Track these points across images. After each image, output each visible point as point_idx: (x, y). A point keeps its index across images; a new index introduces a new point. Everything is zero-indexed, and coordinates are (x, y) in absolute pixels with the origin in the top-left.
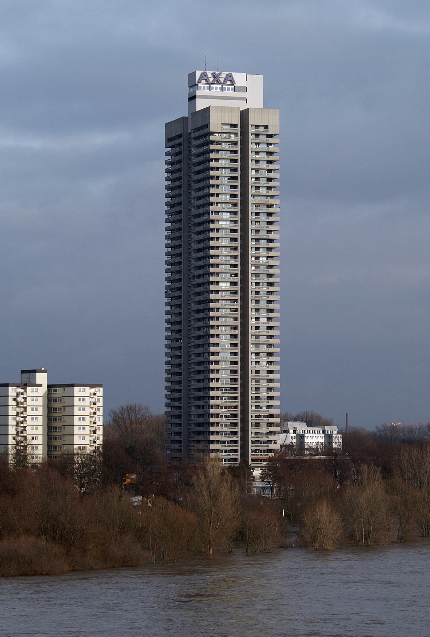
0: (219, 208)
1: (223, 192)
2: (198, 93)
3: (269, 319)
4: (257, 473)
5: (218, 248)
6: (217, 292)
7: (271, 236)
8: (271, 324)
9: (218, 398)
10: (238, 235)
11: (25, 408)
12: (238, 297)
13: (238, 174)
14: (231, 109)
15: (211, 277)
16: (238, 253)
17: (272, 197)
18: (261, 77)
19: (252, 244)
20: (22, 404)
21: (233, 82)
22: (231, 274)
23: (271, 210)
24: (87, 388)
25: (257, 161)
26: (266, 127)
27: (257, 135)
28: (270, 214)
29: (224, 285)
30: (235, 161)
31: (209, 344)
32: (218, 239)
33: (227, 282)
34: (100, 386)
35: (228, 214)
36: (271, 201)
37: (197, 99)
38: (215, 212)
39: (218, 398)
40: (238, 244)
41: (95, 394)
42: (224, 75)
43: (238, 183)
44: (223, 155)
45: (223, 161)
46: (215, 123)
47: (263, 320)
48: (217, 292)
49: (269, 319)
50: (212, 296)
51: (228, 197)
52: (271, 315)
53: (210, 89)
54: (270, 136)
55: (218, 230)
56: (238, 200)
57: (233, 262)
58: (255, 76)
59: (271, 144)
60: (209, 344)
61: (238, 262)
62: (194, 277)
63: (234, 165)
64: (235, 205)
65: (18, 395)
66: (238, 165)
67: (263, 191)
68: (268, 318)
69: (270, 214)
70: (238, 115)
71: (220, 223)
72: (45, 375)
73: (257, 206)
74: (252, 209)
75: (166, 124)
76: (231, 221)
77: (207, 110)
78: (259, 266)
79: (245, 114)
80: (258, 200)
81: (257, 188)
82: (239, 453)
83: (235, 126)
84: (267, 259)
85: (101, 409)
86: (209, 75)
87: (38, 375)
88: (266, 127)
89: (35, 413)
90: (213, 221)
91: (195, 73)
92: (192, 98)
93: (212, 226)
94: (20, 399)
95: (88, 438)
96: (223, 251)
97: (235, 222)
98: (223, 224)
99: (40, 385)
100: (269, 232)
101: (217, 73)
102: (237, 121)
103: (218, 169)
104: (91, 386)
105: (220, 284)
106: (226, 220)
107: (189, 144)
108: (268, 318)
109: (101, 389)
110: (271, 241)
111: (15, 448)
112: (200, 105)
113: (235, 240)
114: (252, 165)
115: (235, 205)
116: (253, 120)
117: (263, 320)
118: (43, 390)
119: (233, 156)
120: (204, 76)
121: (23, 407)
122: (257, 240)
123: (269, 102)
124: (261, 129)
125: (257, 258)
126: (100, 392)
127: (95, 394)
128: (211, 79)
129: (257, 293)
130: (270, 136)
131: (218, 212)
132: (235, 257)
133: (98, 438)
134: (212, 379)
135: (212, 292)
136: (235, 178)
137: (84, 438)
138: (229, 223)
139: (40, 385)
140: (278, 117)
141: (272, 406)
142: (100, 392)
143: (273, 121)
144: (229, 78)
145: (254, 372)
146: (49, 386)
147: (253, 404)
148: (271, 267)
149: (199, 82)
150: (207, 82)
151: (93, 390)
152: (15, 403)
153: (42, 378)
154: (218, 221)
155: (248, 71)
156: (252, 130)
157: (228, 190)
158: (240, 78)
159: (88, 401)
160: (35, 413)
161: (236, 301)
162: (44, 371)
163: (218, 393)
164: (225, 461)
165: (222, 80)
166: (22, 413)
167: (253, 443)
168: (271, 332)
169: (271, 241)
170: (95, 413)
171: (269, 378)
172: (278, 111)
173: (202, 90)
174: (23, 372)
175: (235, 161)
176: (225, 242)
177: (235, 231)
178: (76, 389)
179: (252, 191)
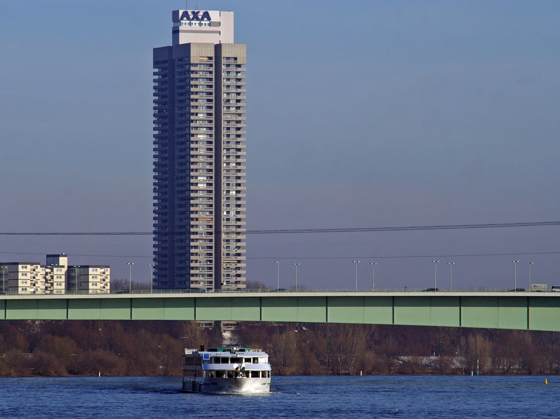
0: (198, 124)
1: (201, 113)
2: (181, 28)
3: (238, 213)
4: (227, 335)
5: (197, 156)
6: (196, 191)
7: (239, 146)
8: (239, 216)
9: (197, 275)
10: (213, 146)
11: (52, 284)
12: (213, 195)
13: (213, 97)
14: (207, 45)
15: (191, 152)
16: (213, 160)
17: (240, 115)
18: (232, 13)
19: (224, 152)
20: (50, 280)
21: (209, 19)
22: (207, 177)
23: (239, 125)
24: (98, 269)
25: (228, 86)
26: (236, 59)
27: (228, 65)
28: (238, 129)
29: (201, 186)
30: (211, 86)
31: (190, 233)
32: (197, 149)
33: (204, 183)
34: (108, 267)
35: (205, 129)
36: (239, 118)
37: (180, 34)
38: (195, 85)
39: (197, 275)
40: (213, 153)
41: (104, 273)
42: (201, 13)
43: (213, 104)
44: (201, 82)
45: (200, 86)
46: (195, 56)
47: (232, 213)
48: (196, 191)
49: (238, 192)
50: (192, 195)
51: (205, 185)
52: (239, 209)
53: (190, 24)
54: (239, 66)
55: (197, 142)
56: (213, 118)
57: (208, 167)
58: (227, 13)
59: (239, 72)
60: (190, 233)
61: (213, 167)
62: (177, 178)
63: (210, 90)
64: (211, 157)
65: (47, 274)
66: (213, 90)
67: (233, 110)
68: (236, 163)
69: (238, 129)
70: (213, 49)
71: (199, 136)
72: (66, 258)
73: (229, 122)
74: (224, 124)
75: (154, 49)
76: (207, 134)
77: (188, 46)
78: (229, 170)
79: (218, 48)
80: (229, 117)
81: (228, 108)
82: (214, 277)
83: (210, 58)
84: (237, 74)
85: (109, 277)
86: (190, 13)
87: (61, 258)
88: (236, 59)
89: (59, 280)
90: (193, 135)
91: (178, 11)
92: (176, 32)
93: (192, 139)
94: (48, 277)
95: (99, 277)
96: (201, 159)
97: (211, 261)
98: (201, 137)
99: (63, 267)
100: (238, 143)
101: (196, 11)
102: (212, 54)
103: (196, 93)
104: (101, 267)
105: (199, 185)
106: (203, 134)
107: (172, 64)
108: (236, 163)
109: (109, 269)
110: (239, 150)
111: (45, 285)
112: (183, 39)
113: (210, 149)
114: (224, 89)
115: (210, 122)
116: (225, 53)
117: (232, 213)
118: (64, 270)
119: (209, 244)
120: (185, 14)
121: (51, 283)
122: (228, 150)
123: (238, 38)
124: (232, 61)
125: (228, 164)
126: (108, 271)
127: (104, 273)
128: (191, 17)
129: (228, 101)
130: (239, 66)
131: (196, 128)
132: (211, 164)
133: (107, 278)
134: (192, 261)
135: (192, 191)
136: (211, 93)
137: (96, 278)
138: (205, 136)
139: (63, 267)
140: (245, 51)
141: (240, 121)
142: (108, 271)
143: (241, 53)
144: (206, 15)
145: (225, 143)
146: (68, 267)
147: (225, 105)
148: (239, 171)
149: (182, 19)
150: (188, 19)
151: (103, 270)
152: (44, 280)
153: (63, 261)
154: (197, 134)
155: (221, 8)
156: (224, 61)
157: (205, 110)
158: (214, 15)
159: (99, 278)
160: (59, 280)
161: (211, 198)
162: (65, 256)
163: (197, 272)
164: (202, 325)
165: (200, 17)
166: (50, 288)
167: (225, 269)
168: (239, 223)
169: (239, 150)
170: (104, 288)
171: (238, 134)
172: (245, 46)
173: (184, 25)
174: (48, 256)
175: (211, 86)
176: (202, 151)
177: (210, 143)
178: (90, 269)
179: (224, 110)
